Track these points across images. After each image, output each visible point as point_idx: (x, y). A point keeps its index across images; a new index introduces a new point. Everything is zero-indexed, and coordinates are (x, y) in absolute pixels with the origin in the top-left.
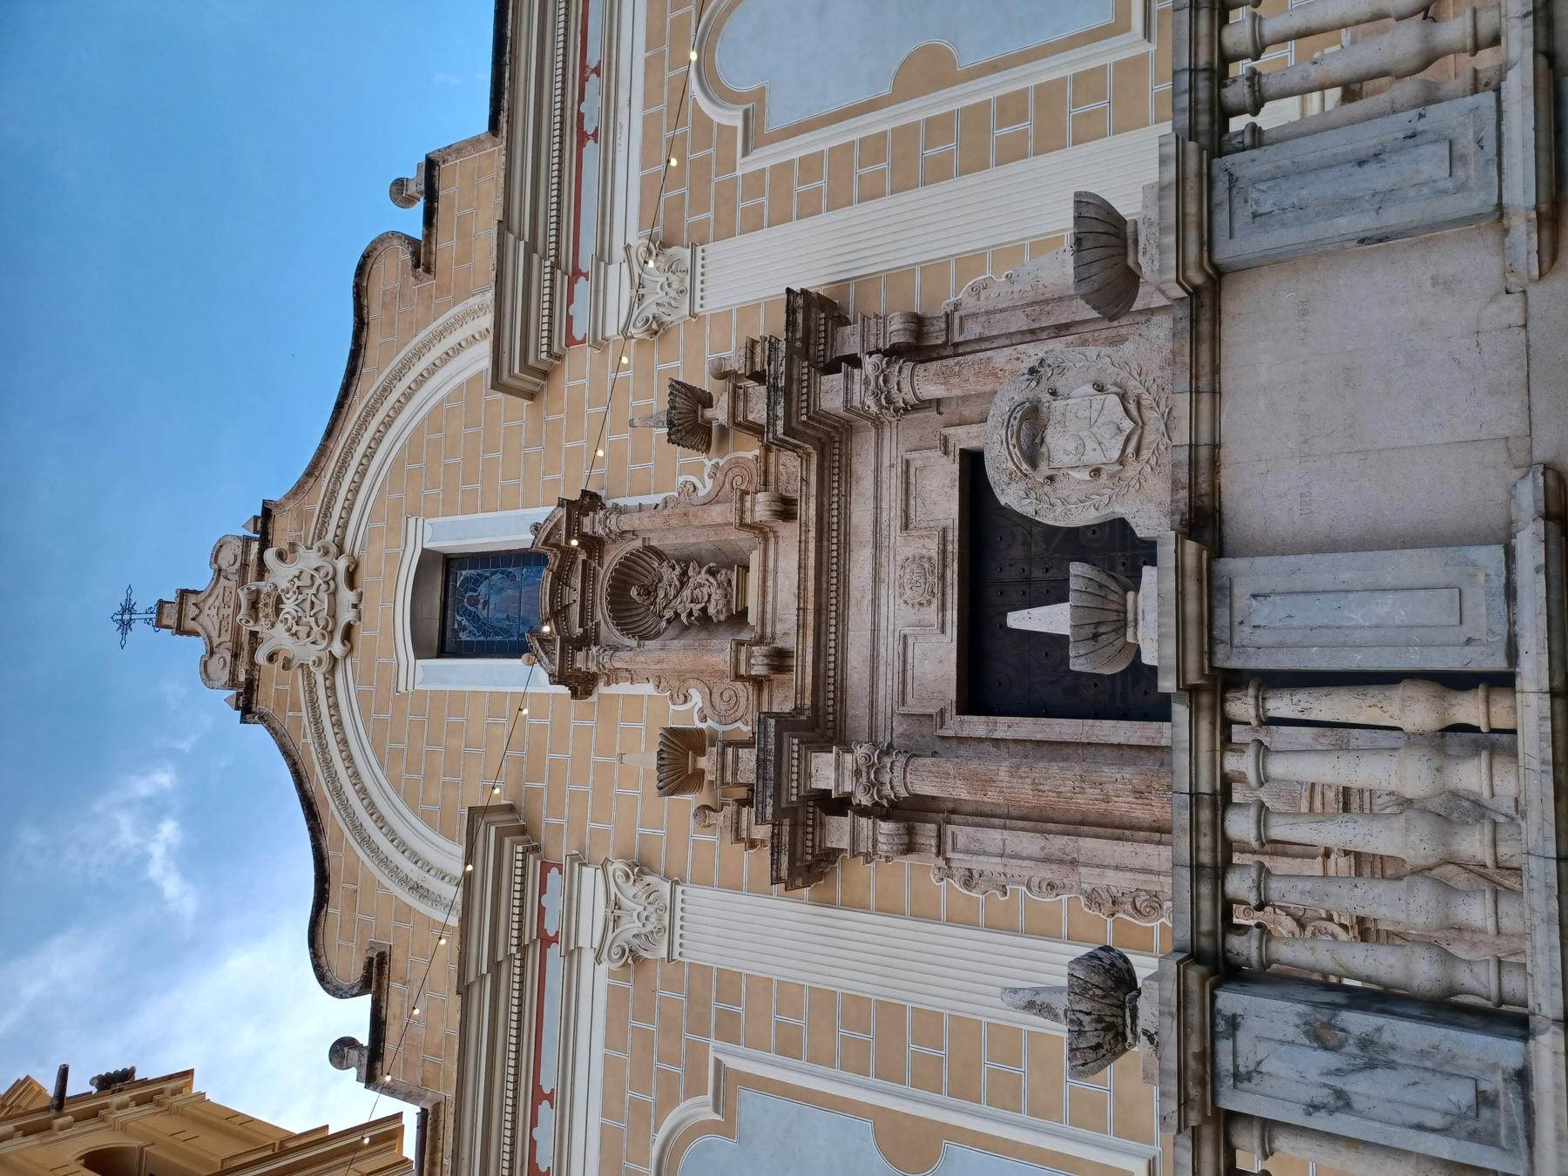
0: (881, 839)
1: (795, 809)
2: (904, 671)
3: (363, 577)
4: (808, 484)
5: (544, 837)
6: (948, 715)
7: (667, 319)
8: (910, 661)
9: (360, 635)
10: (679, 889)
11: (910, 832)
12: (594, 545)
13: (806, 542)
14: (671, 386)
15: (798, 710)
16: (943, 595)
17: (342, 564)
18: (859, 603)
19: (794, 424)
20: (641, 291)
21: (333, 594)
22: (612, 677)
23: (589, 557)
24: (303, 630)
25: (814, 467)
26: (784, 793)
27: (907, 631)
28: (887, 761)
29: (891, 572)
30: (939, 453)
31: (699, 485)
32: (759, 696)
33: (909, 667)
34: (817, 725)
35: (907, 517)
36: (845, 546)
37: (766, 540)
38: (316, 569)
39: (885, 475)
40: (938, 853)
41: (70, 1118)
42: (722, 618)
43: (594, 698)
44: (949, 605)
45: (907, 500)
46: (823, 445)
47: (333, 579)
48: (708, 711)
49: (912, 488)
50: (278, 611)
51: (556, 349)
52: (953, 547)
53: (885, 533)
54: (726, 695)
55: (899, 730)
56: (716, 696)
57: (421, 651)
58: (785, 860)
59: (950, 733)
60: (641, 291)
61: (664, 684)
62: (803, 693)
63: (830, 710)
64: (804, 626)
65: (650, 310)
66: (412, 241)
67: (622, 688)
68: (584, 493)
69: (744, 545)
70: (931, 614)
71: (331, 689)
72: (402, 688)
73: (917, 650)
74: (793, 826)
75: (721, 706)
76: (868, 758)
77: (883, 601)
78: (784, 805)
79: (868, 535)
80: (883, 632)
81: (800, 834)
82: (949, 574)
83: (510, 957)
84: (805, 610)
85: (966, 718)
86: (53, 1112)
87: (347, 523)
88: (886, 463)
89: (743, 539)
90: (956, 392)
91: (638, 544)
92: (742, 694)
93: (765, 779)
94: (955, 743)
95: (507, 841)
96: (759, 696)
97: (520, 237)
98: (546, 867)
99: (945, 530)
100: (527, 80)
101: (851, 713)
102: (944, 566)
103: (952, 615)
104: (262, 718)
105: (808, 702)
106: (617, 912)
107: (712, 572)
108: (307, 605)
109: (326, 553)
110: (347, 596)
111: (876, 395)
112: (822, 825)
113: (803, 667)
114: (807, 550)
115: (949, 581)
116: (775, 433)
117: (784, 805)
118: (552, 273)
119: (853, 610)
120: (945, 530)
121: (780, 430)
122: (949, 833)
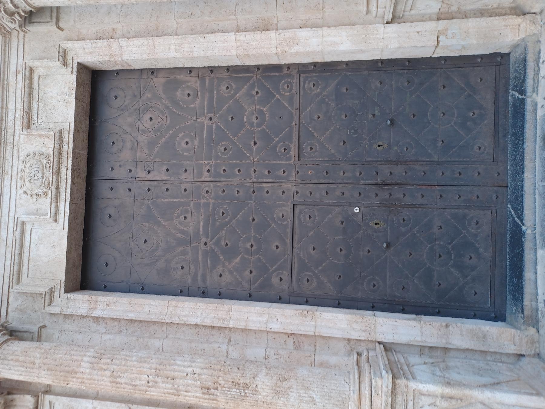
2: (21, 254)
6: (57, 294)
8: (27, 244)
16: (57, 188)
27: (24, 218)
30: (59, 64)
33: (26, 250)
35: (29, 118)
49: (35, 93)
52: (68, 147)
55: (14, 304)
70: (45, 204)
82: (63, 170)
85: (73, 296)
99: (61, 132)
102: (60, 163)
103: (65, 207)
120: (61, 132)
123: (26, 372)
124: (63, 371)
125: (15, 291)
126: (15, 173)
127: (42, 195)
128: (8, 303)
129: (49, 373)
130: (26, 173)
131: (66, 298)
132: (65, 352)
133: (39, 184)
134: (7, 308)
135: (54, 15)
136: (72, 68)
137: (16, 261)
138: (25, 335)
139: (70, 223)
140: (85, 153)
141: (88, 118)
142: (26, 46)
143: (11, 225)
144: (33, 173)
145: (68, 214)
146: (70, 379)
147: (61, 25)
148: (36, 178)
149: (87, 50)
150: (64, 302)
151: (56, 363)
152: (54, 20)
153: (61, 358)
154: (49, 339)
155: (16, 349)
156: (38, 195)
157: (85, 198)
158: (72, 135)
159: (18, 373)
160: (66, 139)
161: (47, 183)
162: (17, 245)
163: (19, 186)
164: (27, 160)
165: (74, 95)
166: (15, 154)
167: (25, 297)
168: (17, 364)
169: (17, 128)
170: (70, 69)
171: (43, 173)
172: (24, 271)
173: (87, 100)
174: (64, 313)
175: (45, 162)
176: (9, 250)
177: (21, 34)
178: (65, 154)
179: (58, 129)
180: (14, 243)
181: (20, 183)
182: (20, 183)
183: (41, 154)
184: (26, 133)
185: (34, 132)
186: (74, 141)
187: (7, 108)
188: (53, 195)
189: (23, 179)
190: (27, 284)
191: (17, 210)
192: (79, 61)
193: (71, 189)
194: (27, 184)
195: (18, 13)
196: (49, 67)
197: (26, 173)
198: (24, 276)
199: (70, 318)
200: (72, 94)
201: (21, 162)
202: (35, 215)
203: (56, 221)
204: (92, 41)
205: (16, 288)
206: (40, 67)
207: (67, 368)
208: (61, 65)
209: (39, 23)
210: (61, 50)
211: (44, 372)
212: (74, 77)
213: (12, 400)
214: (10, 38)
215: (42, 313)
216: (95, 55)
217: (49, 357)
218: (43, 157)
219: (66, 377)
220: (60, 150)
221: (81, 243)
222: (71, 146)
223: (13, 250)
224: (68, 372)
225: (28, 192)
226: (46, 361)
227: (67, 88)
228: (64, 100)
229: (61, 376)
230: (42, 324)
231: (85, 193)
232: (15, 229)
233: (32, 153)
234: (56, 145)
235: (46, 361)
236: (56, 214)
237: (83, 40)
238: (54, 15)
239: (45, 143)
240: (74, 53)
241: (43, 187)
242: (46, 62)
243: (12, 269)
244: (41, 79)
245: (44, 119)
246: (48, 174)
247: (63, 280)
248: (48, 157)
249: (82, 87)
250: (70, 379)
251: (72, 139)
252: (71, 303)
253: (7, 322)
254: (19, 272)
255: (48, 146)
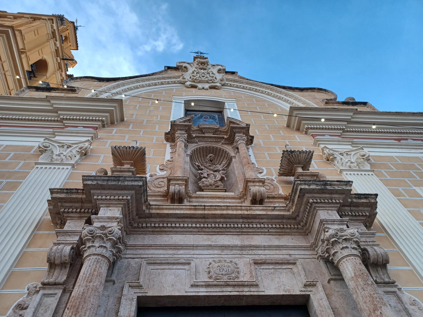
0: (60, 247)
1: (91, 202)
2: (168, 264)
3: (213, 91)
4: (273, 210)
5: (107, 129)
6: (138, 290)
7: (336, 162)
8: (175, 267)
9: (194, 90)
10: (70, 167)
11: (63, 265)
12: (231, 141)
13: (241, 210)
14: (310, 152)
15: (149, 206)
16: (216, 286)
17: (218, 84)
18: (209, 240)
19: (307, 195)
20: (345, 154)
21: (207, 82)
22: (172, 147)
23: (226, 139)
24: (195, 74)
25: (282, 213)
26: (99, 191)
27: (193, 264)
28: (108, 245)
29: (227, 255)
30: (304, 281)
31: (262, 174)
32: (160, 196)
33: (170, 267)
34: (140, 218)
35: (262, 264)
36: (241, 232)
37: (240, 198)
38: (216, 78)
39: (284, 252)
40: (44, 284)
41: (59, 61)
42: (200, 184)
43: (165, 142)
44: (209, 289)
45: (272, 264)
46: (295, 219)
47: (213, 82)
48: (155, 177)
49: (279, 267)
50: (201, 69)
51: (310, 131)
52: (246, 292)
53: (250, 252)
54: (162, 183)
55: (132, 262)
56: (162, 180)
57: (187, 103)
58: (63, 196)
59: (125, 292)
60: (345, 154)
61: (169, 163)
62: (158, 209)
63: (149, 225)
64: (196, 209)
65: (339, 157)
66: (335, 99)
67: (168, 149)
68: (253, 137)
69: (237, 192)
70: (204, 278)
71: (175, 83)
72: (173, 97)
73: (182, 272)
74: (81, 201)
75: (156, 182)
76: (111, 233)
77: (211, 252)
78: (92, 191)
79: (247, 243)
80: (192, 252)
81: (77, 205)
82: (230, 289)
83: (58, 116)
84: (204, 209)
85: (135, 303)
86: (61, 57)
87: (232, 87)
88: (292, 252)
89: (241, 186)
90: (351, 284)
91: (232, 154)
92: (162, 189)
93: (108, 180)
94: (118, 295)
95: (108, 114)
96: (160, 196)
97: (353, 118)
98: (96, 128)
99: (257, 286)
100: (415, 120)
101: (146, 237)
102: (234, 286)
103: (202, 292)
104: (165, 70)
105: (154, 211)
106: (66, 147)
107: (222, 179)
108: (203, 75)
109: (221, 80)
110: (207, 86)
111: (336, 235)
112: (80, 218)
113: (173, 209)
114: (237, 210)
115: (225, 289)
116: (301, 184)
117: (92, 191)
118: (340, 129)
119: (205, 237)
120: (257, 286)
121: (303, 187)
122: (56, 291)
123: (85, 277)
124: (79, 305)
125: (142, 262)
126: (223, 256)
127: (209, 275)
128: (135, 258)
129: (81, 294)
130: (224, 263)
131: (134, 298)
132: (94, 303)
133: (217, 272)
134: (131, 258)
135: (337, 277)
136: (304, 291)
137: (163, 261)
138: (110, 271)
139: (190, 296)
140: (244, 303)
141: (270, 304)
142: (309, 259)
143: (188, 256)
144: (225, 268)
145: (197, 295)
146: (72, 310)
147: (332, 282)
148: (221, 270)
149: (321, 301)
150: (131, 296)
151: (87, 298)
152: (333, 277)
153: (90, 301)
154: (105, 288)
155: (103, 269)
156: (209, 272)
157: (209, 305)
158: (256, 294)
159: (86, 271)
160: (252, 289)
161: (218, 278)
162: (174, 261)
163: (215, 259)
164: (233, 263)
165: (285, 294)
166: (235, 256)
167: (137, 268)
168: (93, 270)
169: (253, 256)
170: (303, 289)
171: (225, 275)
172: (155, 266)
173: (283, 303)
174: (122, 297)
175: (233, 275)
176: (171, 256)
177: (316, 257)
178: (241, 289)
179: (258, 283)
180: (176, 259)
181: (217, 260)
182: (217, 260)
183: (238, 273)
184: (251, 262)
185: (253, 267)
186: (252, 295)
187: (265, 250)
188: (211, 283)
189: (220, 261)
190: (146, 269)
191: (198, 259)
192: (311, 295)
193: (216, 296)
194: (217, 265)
195: (330, 255)
196: (300, 276)
197: (224, 263)
198: (152, 267)
199: (118, 302)
200: (286, 292)
201: (231, 259)
202: (195, 271)
203: (192, 286)
204: (329, 305)
205: (144, 263)
206: (298, 269)
207: (81, 307)
208: (304, 283)
209: (328, 268)
210: (315, 282)
211: (82, 289)
212: (297, 292)
213: (65, 267)
214: (310, 250)
215: (124, 281)
216: (320, 308)
217: (93, 292)
218: (237, 274)
219: (75, 306)
220: (243, 286)
221: (174, 305)
222: (248, 294)
223: (171, 259)
224: (78, 308)
225: (211, 266)
226: (90, 290)
227: (289, 288)
228: (280, 287)
229: (76, 303)
230: (116, 282)
231: (213, 305)
232: (185, 259)
233: (238, 266)
234: (247, 283)
235: (90, 290)
236: (197, 286)
237: (327, 298)
238: (337, 277)
239: (247, 275)
240: (316, 292)
241: (215, 275)
242: (302, 273)
243: (158, 259)
244: (290, 270)
245: (263, 273)
246: (225, 278)
247: (147, 295)
248: (237, 277)
249: (292, 299)
250: (72, 310)
251: (253, 294)
252: (129, 302)
253: (121, 259)
254: (156, 264)
255: (245, 278)
